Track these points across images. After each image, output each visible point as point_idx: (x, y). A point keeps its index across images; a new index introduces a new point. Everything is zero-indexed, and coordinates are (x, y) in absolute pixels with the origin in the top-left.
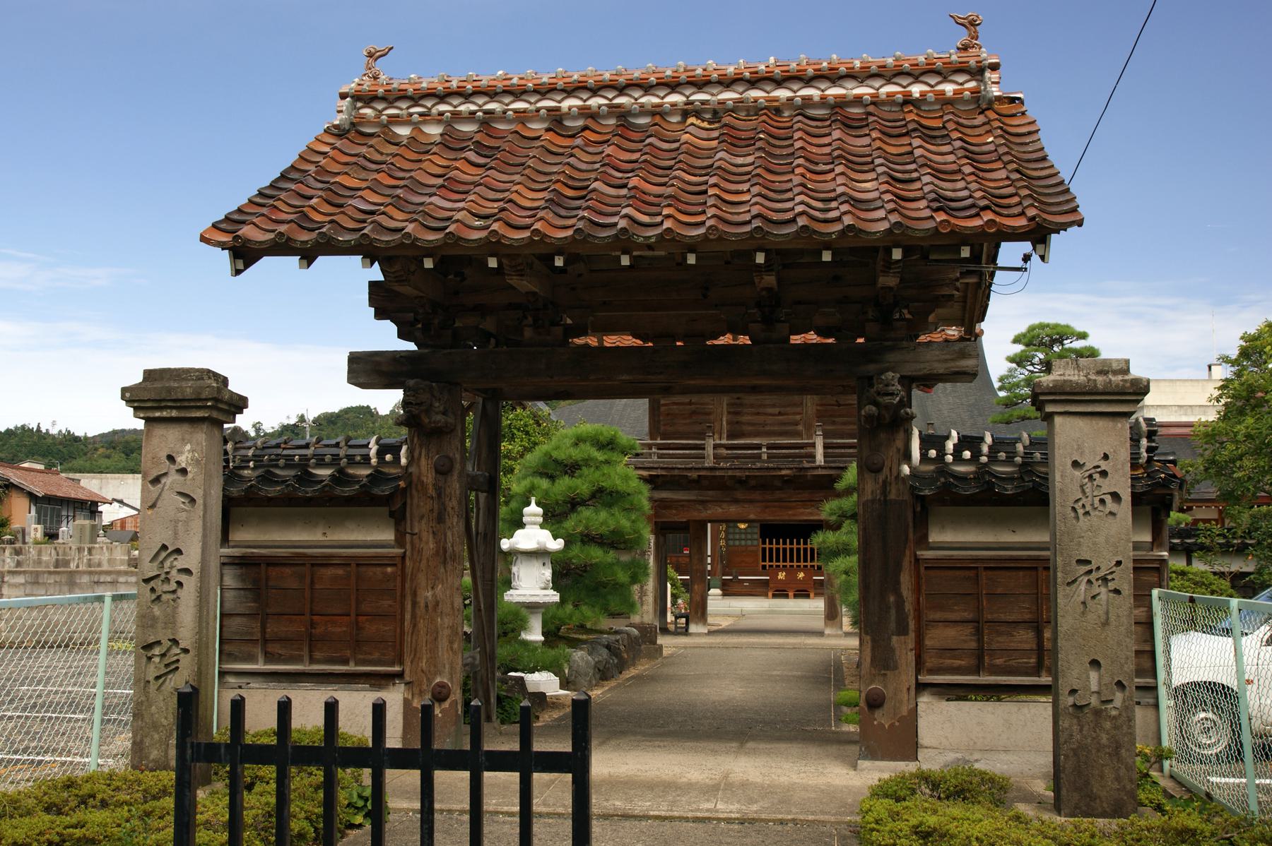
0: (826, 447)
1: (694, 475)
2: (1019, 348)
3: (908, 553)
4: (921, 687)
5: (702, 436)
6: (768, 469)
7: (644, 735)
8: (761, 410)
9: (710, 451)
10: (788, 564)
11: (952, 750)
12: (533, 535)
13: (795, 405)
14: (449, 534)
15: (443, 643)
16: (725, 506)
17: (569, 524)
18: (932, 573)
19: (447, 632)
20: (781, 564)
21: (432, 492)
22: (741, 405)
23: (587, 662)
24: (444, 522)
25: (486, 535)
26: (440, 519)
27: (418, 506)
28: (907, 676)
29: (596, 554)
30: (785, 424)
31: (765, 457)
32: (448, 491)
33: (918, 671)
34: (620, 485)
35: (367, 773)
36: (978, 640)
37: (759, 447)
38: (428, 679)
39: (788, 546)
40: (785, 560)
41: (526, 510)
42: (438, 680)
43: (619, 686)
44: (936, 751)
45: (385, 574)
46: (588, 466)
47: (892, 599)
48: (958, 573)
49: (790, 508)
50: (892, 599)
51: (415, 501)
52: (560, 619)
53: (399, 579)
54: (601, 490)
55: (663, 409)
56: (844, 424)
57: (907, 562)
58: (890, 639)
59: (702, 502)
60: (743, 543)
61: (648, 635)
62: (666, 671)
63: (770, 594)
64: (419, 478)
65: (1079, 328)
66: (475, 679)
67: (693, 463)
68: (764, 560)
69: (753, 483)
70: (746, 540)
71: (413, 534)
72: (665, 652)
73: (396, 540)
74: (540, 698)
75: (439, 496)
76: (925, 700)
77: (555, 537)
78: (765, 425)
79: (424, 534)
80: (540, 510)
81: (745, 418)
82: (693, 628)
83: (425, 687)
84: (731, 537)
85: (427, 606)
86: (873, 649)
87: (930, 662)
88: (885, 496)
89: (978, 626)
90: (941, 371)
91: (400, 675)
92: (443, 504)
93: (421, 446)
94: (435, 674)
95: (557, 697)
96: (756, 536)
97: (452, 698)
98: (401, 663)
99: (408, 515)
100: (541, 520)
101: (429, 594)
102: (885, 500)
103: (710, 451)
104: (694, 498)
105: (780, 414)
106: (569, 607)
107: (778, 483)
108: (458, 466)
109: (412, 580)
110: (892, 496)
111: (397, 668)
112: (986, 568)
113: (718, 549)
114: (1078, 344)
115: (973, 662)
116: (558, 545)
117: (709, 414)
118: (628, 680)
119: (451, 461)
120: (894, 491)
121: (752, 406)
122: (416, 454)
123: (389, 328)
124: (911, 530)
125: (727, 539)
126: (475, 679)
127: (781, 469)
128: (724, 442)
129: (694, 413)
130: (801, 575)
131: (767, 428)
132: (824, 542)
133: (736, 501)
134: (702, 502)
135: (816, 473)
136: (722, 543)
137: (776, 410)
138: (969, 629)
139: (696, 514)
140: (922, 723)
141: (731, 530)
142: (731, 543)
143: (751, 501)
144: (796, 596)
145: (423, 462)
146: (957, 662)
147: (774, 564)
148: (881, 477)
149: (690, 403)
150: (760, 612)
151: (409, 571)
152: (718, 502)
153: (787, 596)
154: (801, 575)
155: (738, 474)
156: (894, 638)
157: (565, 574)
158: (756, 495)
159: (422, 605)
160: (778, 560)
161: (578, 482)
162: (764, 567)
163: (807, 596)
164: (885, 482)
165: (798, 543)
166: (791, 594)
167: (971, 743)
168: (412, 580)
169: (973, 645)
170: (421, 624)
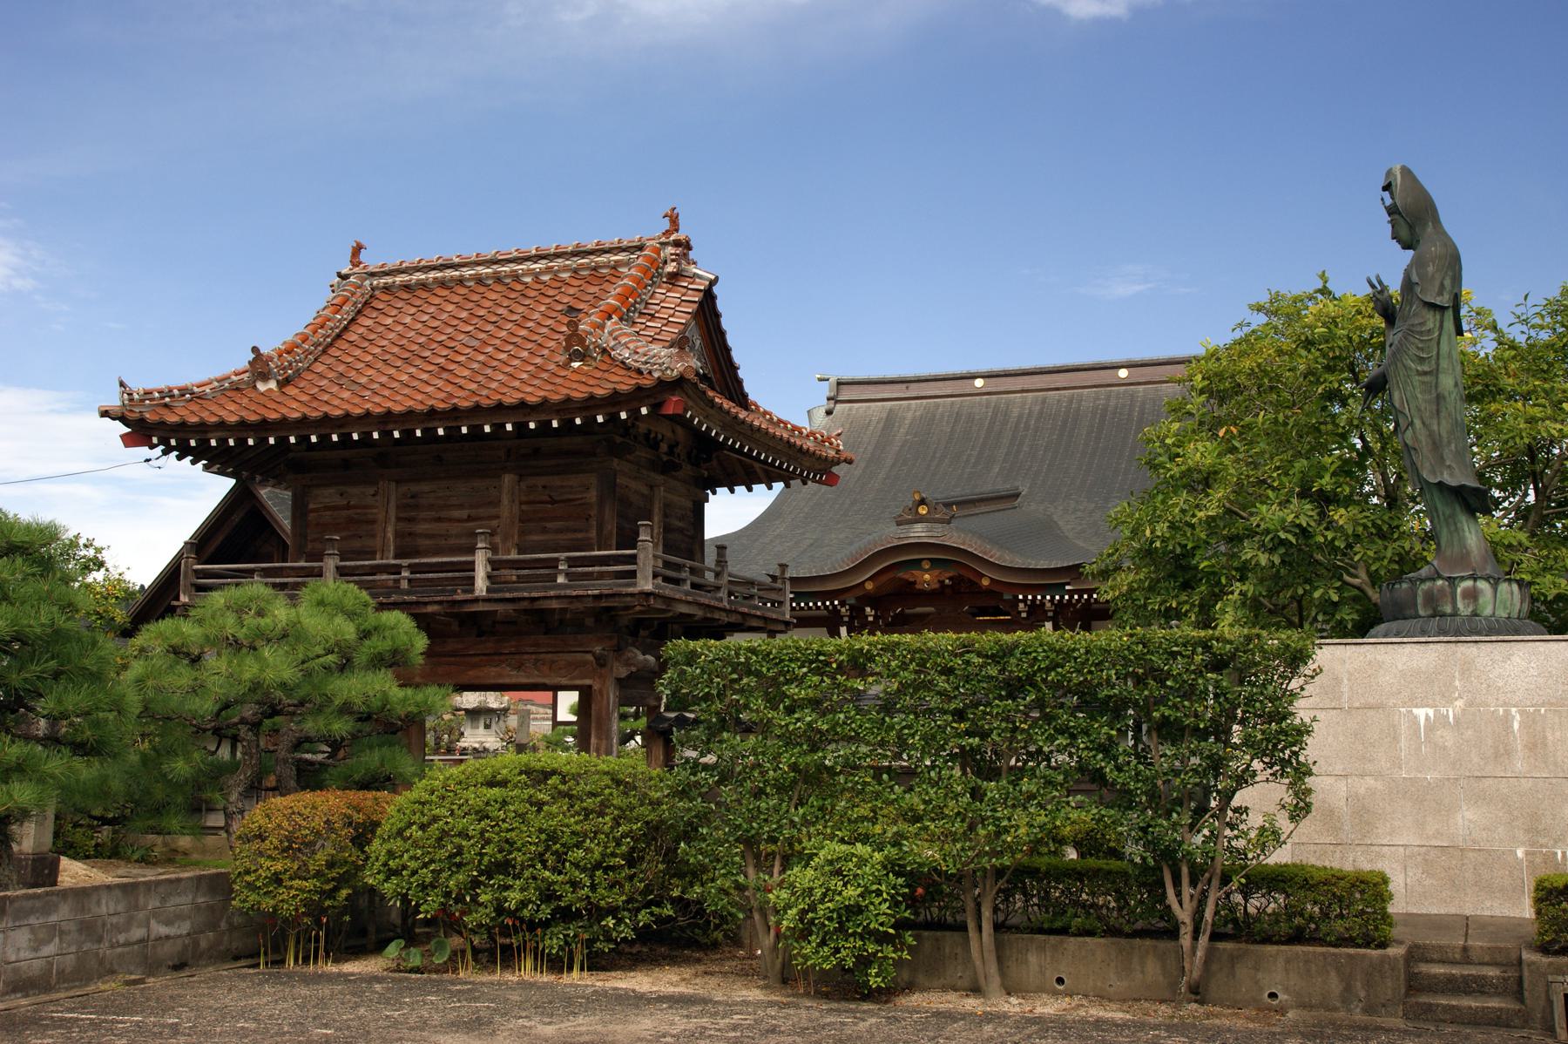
8: (443, 514)
13: (490, 503)
22: (417, 507)
31: (404, 585)
55: (312, 516)
62: (1136, 960)
78: (446, 536)
81: (422, 527)
121: (431, 507)
123: (759, 488)
127: (426, 604)
131: (452, 541)
137: (464, 514)
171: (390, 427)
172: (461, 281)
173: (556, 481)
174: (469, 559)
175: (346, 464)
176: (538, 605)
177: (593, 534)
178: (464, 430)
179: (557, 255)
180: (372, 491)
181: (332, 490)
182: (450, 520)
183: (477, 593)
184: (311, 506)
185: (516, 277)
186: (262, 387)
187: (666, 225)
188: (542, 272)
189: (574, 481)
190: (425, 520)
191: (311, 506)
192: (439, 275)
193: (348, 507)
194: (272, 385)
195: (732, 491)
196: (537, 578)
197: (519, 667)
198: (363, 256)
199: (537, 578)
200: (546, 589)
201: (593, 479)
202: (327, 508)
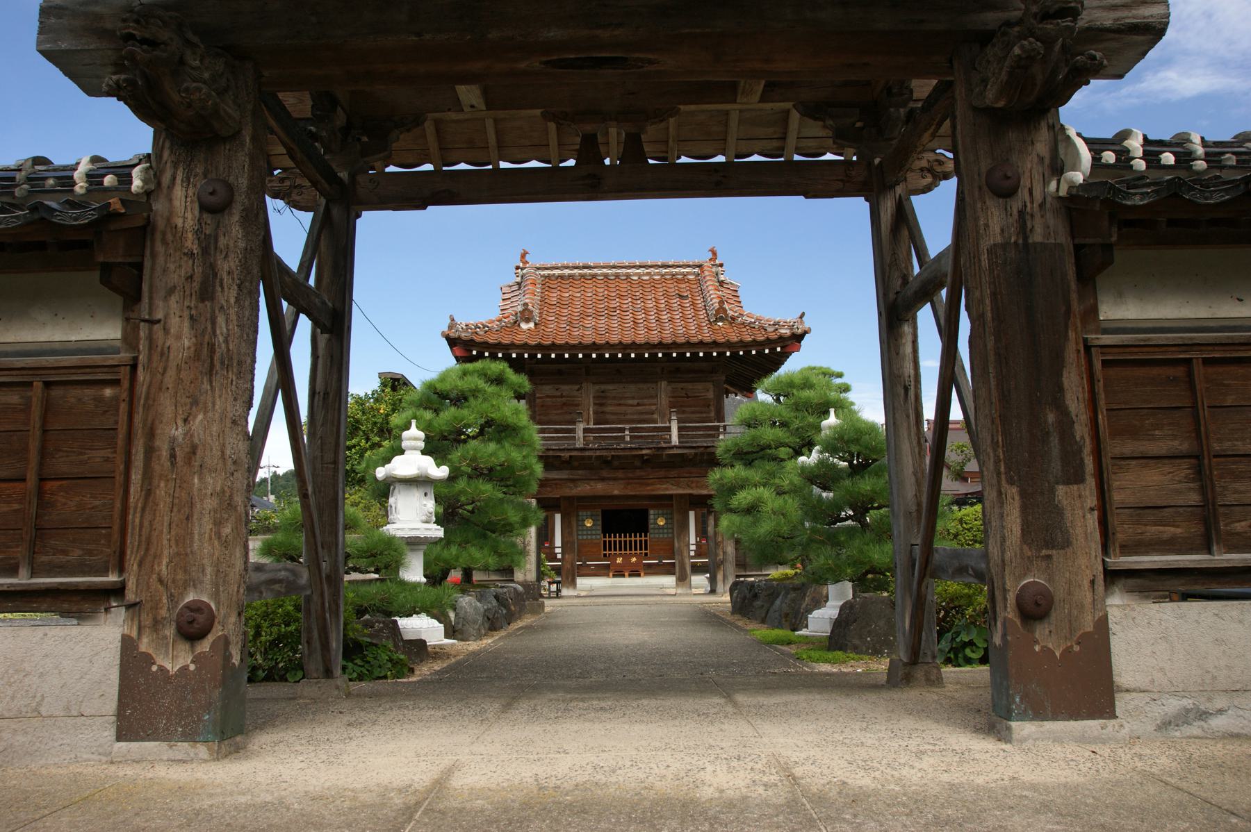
0: (680, 429)
1: (566, 455)
3: (1071, 335)
4: (1113, 576)
5: (574, 423)
6: (631, 449)
7: (568, 690)
9: (580, 434)
11: (1174, 694)
12: (412, 461)
13: (651, 397)
14: (221, 320)
15: (203, 526)
16: (592, 483)
17: (456, 455)
18: (1112, 372)
19: (210, 504)
21: (191, 243)
22: (605, 398)
23: (476, 608)
24: (212, 298)
25: (326, 394)
26: (206, 292)
27: (165, 270)
28: (1086, 558)
29: (487, 489)
32: (222, 241)
33: (1105, 550)
34: (511, 420)
36: (1203, 491)
37: (623, 430)
38: (171, 597)
41: (405, 434)
42: (191, 597)
43: (509, 635)
44: (1145, 696)
45: (99, 400)
46: (476, 397)
47: (1051, 418)
48: (1155, 371)
49: (648, 485)
50: (1051, 418)
51: (161, 260)
52: (445, 561)
53: (123, 407)
54: (489, 423)
57: (1072, 353)
58: (1052, 491)
61: (532, 594)
64: (169, 220)
65: (836, 368)
66: (308, 612)
69: (616, 463)
71: (152, 322)
72: (547, 609)
73: (125, 339)
74: (419, 647)
75: (205, 251)
76: (1117, 604)
77: (438, 465)
78: (625, 414)
79: (174, 322)
80: (422, 435)
81: (609, 409)
82: (565, 592)
83: (164, 612)
85: (173, 456)
86: (1024, 509)
87: (1123, 531)
88: (1026, 238)
89: (1200, 462)
90: (1108, 23)
91: (117, 591)
92: (213, 267)
93: (175, 166)
94: (186, 586)
95: (441, 647)
97: (217, 632)
98: (121, 570)
99: (145, 287)
100: (422, 445)
101: (179, 432)
102: (1026, 244)
103: (580, 434)
105: (638, 405)
106: (454, 550)
107: (637, 463)
108: (241, 200)
109: (147, 408)
110: (1037, 237)
111: (113, 578)
112: (1206, 362)
114: (838, 381)
115: (1195, 529)
116: (442, 472)
117: (577, 405)
118: (519, 629)
119: (230, 189)
120: (1039, 229)
121: (614, 398)
122: (166, 179)
124: (1074, 296)
126: (308, 612)
128: (592, 426)
130: (634, 559)
131: (628, 417)
132: (721, 479)
133: (603, 479)
135: (672, 452)
137: (635, 402)
138: (1183, 470)
140: (1118, 645)
143: (615, 479)
144: (630, 575)
145: (179, 192)
146: (1169, 531)
148: (1015, 206)
151: (141, 390)
153: (623, 576)
154: (634, 559)
155: (604, 453)
156: (1061, 490)
157: (450, 512)
158: (620, 474)
159: (165, 453)
161: (465, 412)
163: (639, 575)
164: (1021, 213)
167: (1208, 679)
168: (147, 408)
169: (1194, 498)
170: (162, 491)
172: (594, 276)
173: (689, 386)
175: (560, 372)
177: (712, 414)
178: (633, 355)
179: (651, 267)
180: (577, 387)
185: (628, 276)
186: (524, 326)
187: (710, 255)
193: (562, 396)
194: (531, 325)
196: (709, 436)
197: (677, 485)
198: (527, 258)
199: (709, 436)
201: (710, 385)
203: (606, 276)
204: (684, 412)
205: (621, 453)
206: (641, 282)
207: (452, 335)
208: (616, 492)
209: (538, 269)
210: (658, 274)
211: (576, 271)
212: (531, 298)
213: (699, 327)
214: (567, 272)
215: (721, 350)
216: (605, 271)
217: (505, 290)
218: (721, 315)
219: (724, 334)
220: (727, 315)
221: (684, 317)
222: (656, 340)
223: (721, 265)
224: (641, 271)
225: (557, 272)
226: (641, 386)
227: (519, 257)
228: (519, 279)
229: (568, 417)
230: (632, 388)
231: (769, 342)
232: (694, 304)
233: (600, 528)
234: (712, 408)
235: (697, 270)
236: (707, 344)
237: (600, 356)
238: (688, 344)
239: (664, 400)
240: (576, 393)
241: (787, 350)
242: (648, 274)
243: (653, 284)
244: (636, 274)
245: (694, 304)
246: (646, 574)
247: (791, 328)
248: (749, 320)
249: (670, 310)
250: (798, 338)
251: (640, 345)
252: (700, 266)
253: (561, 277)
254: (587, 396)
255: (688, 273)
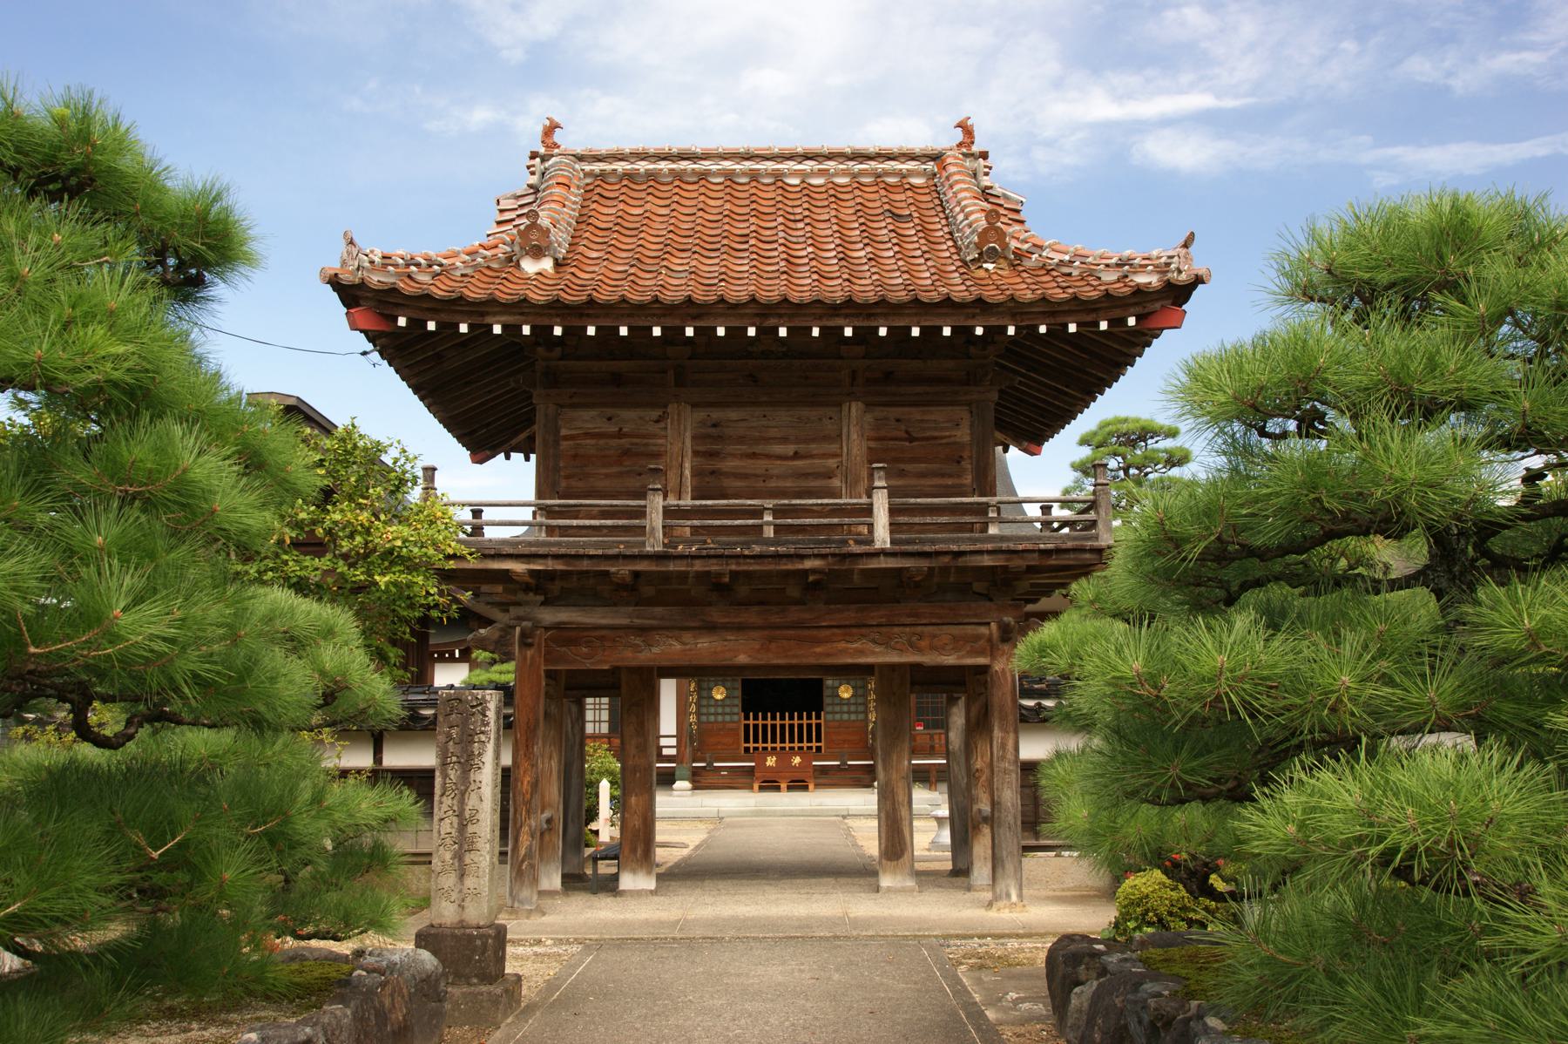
0: (893, 511)
1: (623, 570)
2: (1086, 452)
5: (642, 495)
6: (777, 556)
8: (759, 449)
9: (656, 520)
10: (778, 745)
13: (826, 438)
16: (687, 637)
20: (769, 745)
22: (720, 438)
30: (806, 475)
31: (769, 532)
35: (673, 752)
37: (757, 513)
39: (796, 722)
40: (774, 741)
55: (564, 444)
56: (922, 475)
59: (642, 630)
60: (720, 718)
63: (756, 786)
67: (620, 545)
68: (747, 741)
70: (724, 714)
78: (767, 477)
81: (729, 464)
84: (704, 710)
96: (736, 710)
103: (656, 520)
104: (625, 621)
105: (796, 456)
107: (794, 591)
113: (686, 726)
114: (1167, 444)
117: (657, 456)
121: (741, 440)
125: (698, 714)
127: (802, 557)
128: (687, 502)
129: (626, 453)
130: (797, 760)
131: (773, 484)
133: (711, 628)
134: (642, 630)
136: (693, 719)
137: (790, 449)
139: (628, 653)
141: (704, 702)
142: (704, 718)
143: (740, 628)
144: (790, 788)
147: (760, 745)
149: (620, 434)
150: (742, 814)
152: (676, 629)
153: (778, 789)
155: (714, 567)
158: (751, 616)
160: (765, 741)
162: (747, 750)
163: (805, 788)
165: (809, 717)
166: (783, 785)
171: (772, 322)
172: (703, 176)
173: (916, 414)
174: (642, 503)
176: (961, 561)
177: (968, 479)
179: (830, 157)
180: (655, 414)
181: (593, 413)
182: (768, 456)
183: (878, 545)
184: (564, 432)
185: (778, 176)
186: (530, 266)
187: (959, 135)
188: (813, 174)
189: (938, 415)
190: (734, 456)
191: (564, 432)
192: (674, 166)
193: (620, 434)
194: (547, 264)
195: (508, 457)
196: (960, 527)
197: (886, 643)
198: (558, 136)
199: (960, 527)
200: (974, 541)
201: (962, 413)
202: (588, 435)
203: (729, 175)
204: (902, 474)
205: (754, 567)
206: (806, 188)
207: (346, 278)
208: (742, 659)
209: (580, 158)
210: (844, 173)
211: (664, 166)
212: (557, 218)
213: (940, 274)
214: (643, 166)
215: (994, 321)
216: (727, 164)
217: (505, 205)
218: (992, 246)
219: (995, 280)
220: (1005, 246)
221: (902, 254)
222: (839, 296)
223: (984, 155)
224: (808, 166)
225: (620, 166)
226: (805, 412)
227: (540, 129)
228: (534, 180)
229: (633, 483)
230: (782, 418)
231: (1110, 303)
232: (924, 230)
233: (738, 702)
234: (966, 464)
235: (930, 166)
236: (962, 306)
237: (705, 333)
238: (917, 306)
239: (855, 445)
240: (653, 428)
241: (1152, 323)
242: (822, 172)
243: (834, 194)
244: (795, 173)
245: (924, 230)
246: (817, 786)
247: (1163, 269)
248: (1057, 257)
249: (871, 240)
250: (1177, 293)
251: (800, 306)
252: (937, 157)
253: (630, 176)
254: (679, 438)
255: (911, 173)
